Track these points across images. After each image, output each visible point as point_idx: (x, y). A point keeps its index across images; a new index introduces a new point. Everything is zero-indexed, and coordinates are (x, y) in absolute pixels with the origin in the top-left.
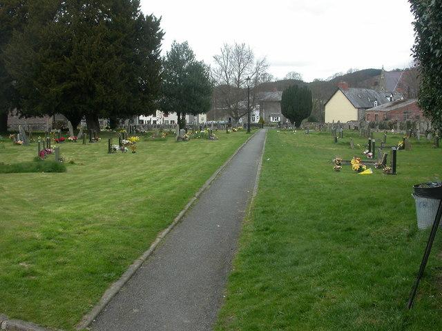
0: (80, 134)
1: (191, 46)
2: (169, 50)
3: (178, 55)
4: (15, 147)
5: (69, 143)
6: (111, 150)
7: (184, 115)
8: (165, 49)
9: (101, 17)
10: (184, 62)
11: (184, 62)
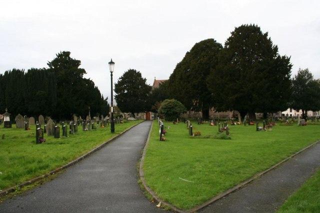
0: (244, 122)
1: (310, 71)
2: (297, 74)
3: (302, 76)
4: (210, 126)
5: (285, 128)
6: (258, 130)
7: (306, 112)
8: (294, 74)
9: (257, 59)
10: (306, 80)
11: (306, 80)
